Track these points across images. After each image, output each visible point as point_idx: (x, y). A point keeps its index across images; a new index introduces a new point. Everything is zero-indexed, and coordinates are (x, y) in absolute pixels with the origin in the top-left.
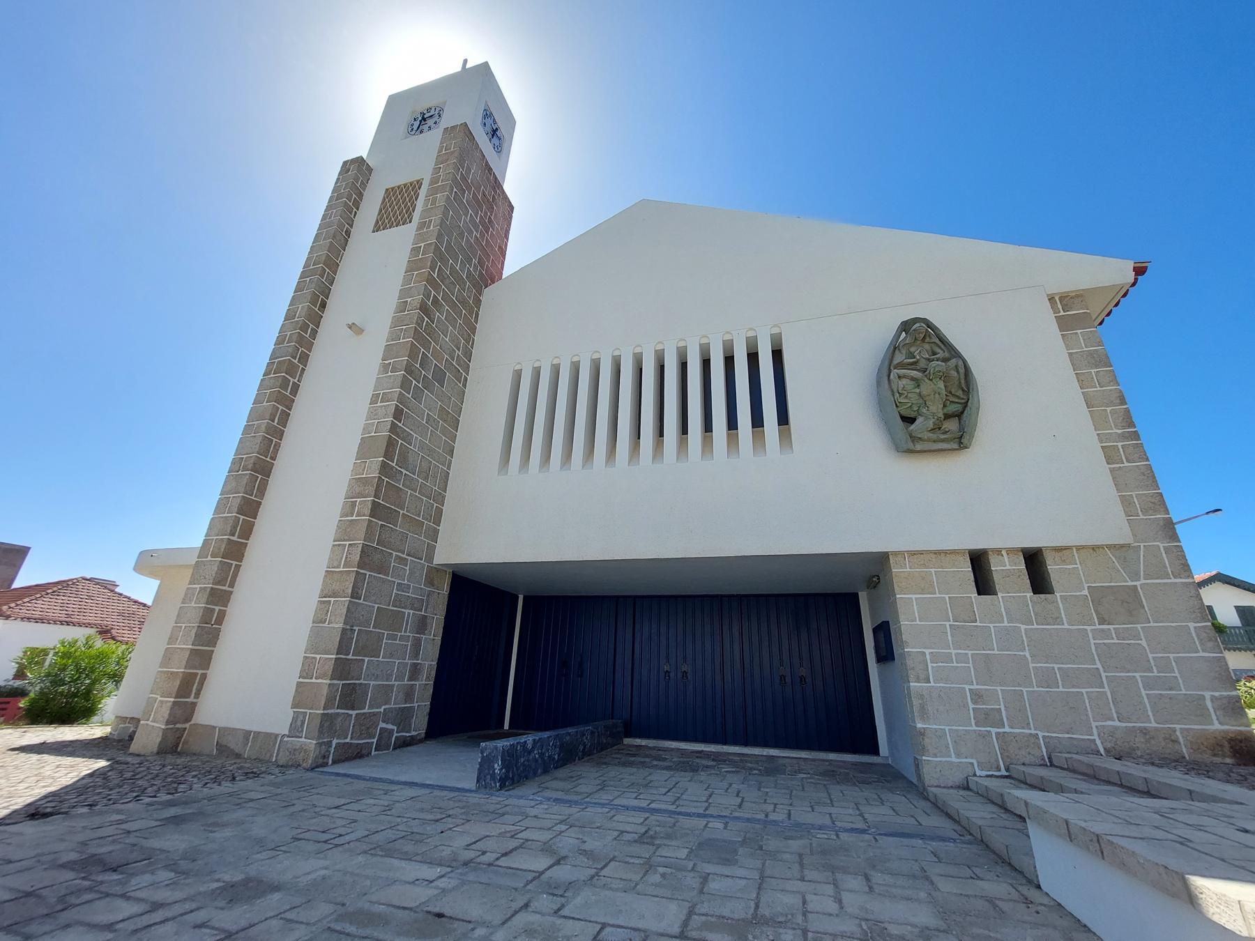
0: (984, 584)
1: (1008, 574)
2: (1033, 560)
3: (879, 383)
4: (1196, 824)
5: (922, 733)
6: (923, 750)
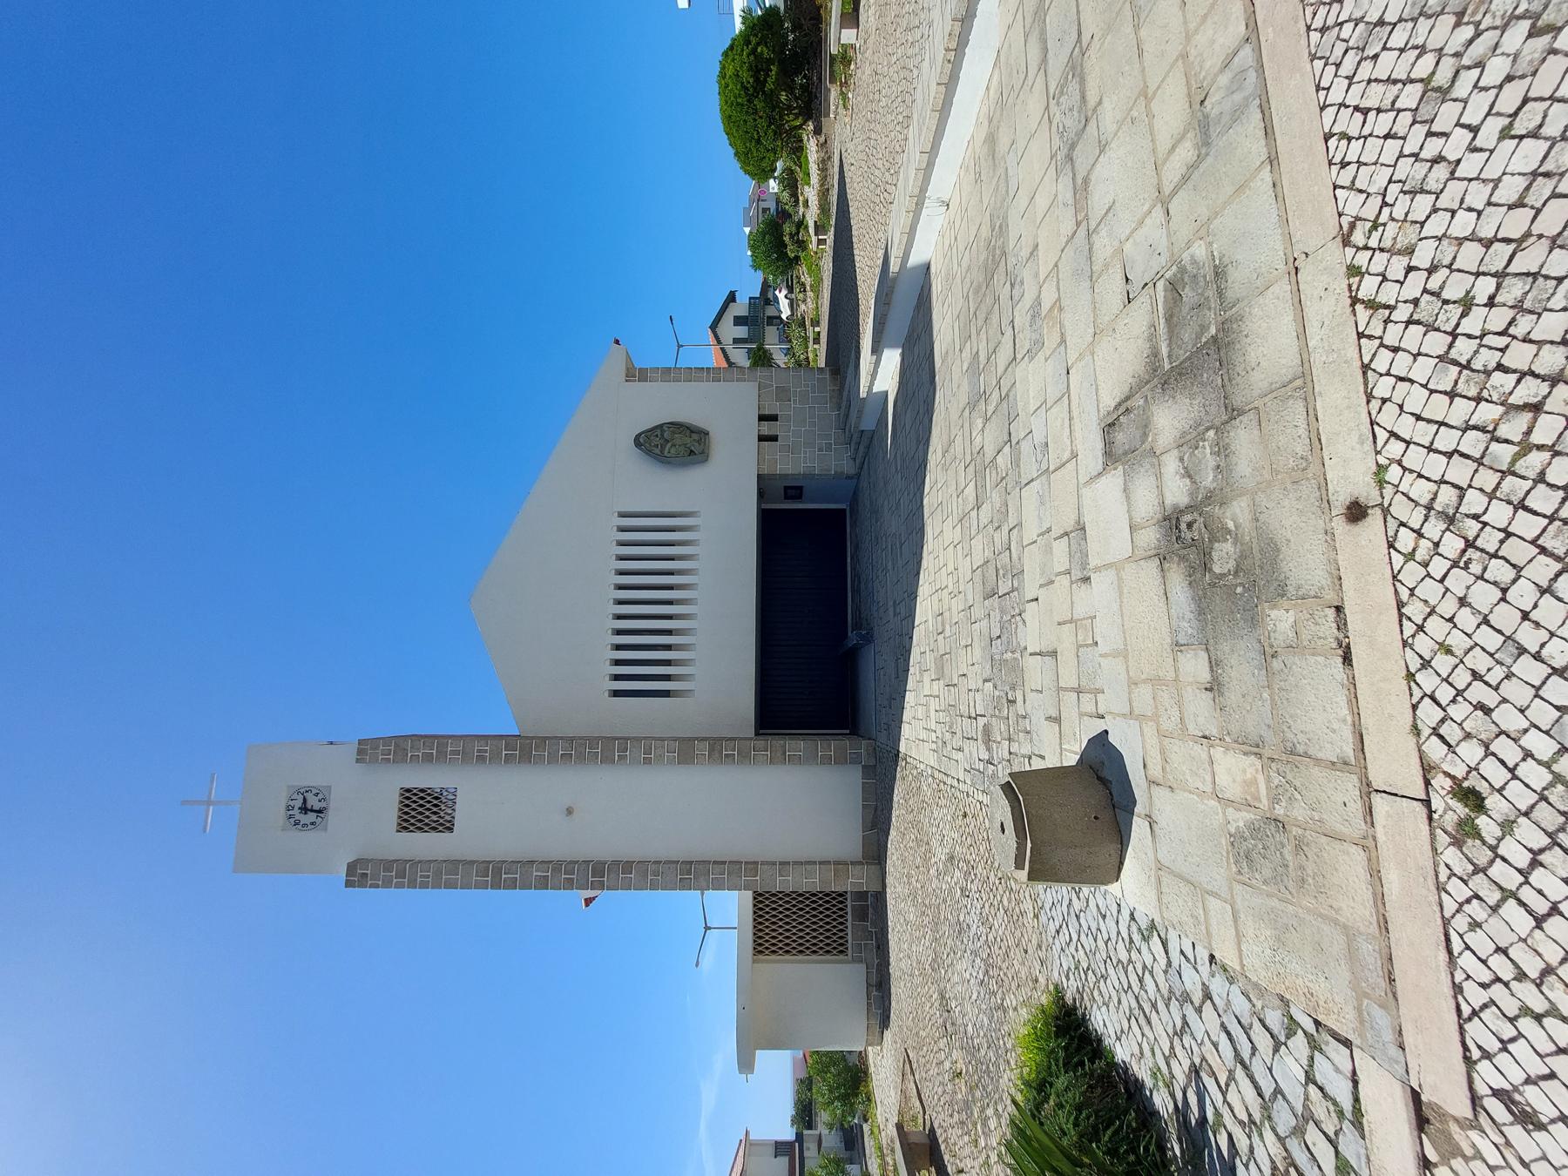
0: (774, 438)
1: (769, 429)
2: (762, 418)
3: (669, 463)
4: (1362, 389)
5: (836, 472)
6: (842, 473)
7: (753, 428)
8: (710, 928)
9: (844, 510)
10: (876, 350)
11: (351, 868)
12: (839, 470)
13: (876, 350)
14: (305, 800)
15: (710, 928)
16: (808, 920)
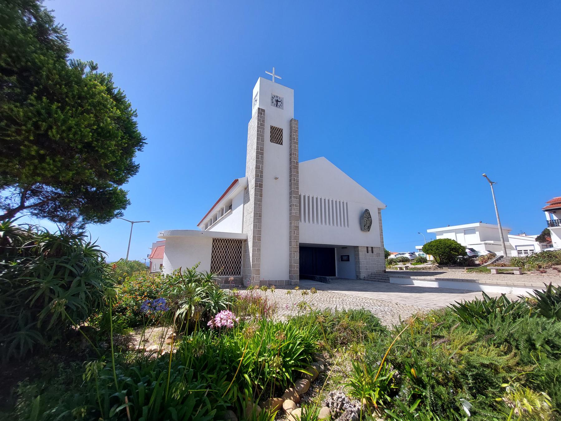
2: (372, 248)
7: (370, 245)
8: (132, 224)
9: (335, 276)
10: (437, 280)
11: (263, 111)
12: (361, 273)
13: (437, 280)
14: (280, 102)
15: (132, 224)
16: (222, 260)
